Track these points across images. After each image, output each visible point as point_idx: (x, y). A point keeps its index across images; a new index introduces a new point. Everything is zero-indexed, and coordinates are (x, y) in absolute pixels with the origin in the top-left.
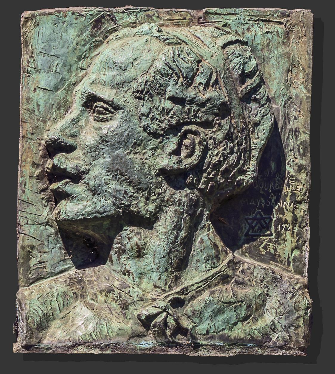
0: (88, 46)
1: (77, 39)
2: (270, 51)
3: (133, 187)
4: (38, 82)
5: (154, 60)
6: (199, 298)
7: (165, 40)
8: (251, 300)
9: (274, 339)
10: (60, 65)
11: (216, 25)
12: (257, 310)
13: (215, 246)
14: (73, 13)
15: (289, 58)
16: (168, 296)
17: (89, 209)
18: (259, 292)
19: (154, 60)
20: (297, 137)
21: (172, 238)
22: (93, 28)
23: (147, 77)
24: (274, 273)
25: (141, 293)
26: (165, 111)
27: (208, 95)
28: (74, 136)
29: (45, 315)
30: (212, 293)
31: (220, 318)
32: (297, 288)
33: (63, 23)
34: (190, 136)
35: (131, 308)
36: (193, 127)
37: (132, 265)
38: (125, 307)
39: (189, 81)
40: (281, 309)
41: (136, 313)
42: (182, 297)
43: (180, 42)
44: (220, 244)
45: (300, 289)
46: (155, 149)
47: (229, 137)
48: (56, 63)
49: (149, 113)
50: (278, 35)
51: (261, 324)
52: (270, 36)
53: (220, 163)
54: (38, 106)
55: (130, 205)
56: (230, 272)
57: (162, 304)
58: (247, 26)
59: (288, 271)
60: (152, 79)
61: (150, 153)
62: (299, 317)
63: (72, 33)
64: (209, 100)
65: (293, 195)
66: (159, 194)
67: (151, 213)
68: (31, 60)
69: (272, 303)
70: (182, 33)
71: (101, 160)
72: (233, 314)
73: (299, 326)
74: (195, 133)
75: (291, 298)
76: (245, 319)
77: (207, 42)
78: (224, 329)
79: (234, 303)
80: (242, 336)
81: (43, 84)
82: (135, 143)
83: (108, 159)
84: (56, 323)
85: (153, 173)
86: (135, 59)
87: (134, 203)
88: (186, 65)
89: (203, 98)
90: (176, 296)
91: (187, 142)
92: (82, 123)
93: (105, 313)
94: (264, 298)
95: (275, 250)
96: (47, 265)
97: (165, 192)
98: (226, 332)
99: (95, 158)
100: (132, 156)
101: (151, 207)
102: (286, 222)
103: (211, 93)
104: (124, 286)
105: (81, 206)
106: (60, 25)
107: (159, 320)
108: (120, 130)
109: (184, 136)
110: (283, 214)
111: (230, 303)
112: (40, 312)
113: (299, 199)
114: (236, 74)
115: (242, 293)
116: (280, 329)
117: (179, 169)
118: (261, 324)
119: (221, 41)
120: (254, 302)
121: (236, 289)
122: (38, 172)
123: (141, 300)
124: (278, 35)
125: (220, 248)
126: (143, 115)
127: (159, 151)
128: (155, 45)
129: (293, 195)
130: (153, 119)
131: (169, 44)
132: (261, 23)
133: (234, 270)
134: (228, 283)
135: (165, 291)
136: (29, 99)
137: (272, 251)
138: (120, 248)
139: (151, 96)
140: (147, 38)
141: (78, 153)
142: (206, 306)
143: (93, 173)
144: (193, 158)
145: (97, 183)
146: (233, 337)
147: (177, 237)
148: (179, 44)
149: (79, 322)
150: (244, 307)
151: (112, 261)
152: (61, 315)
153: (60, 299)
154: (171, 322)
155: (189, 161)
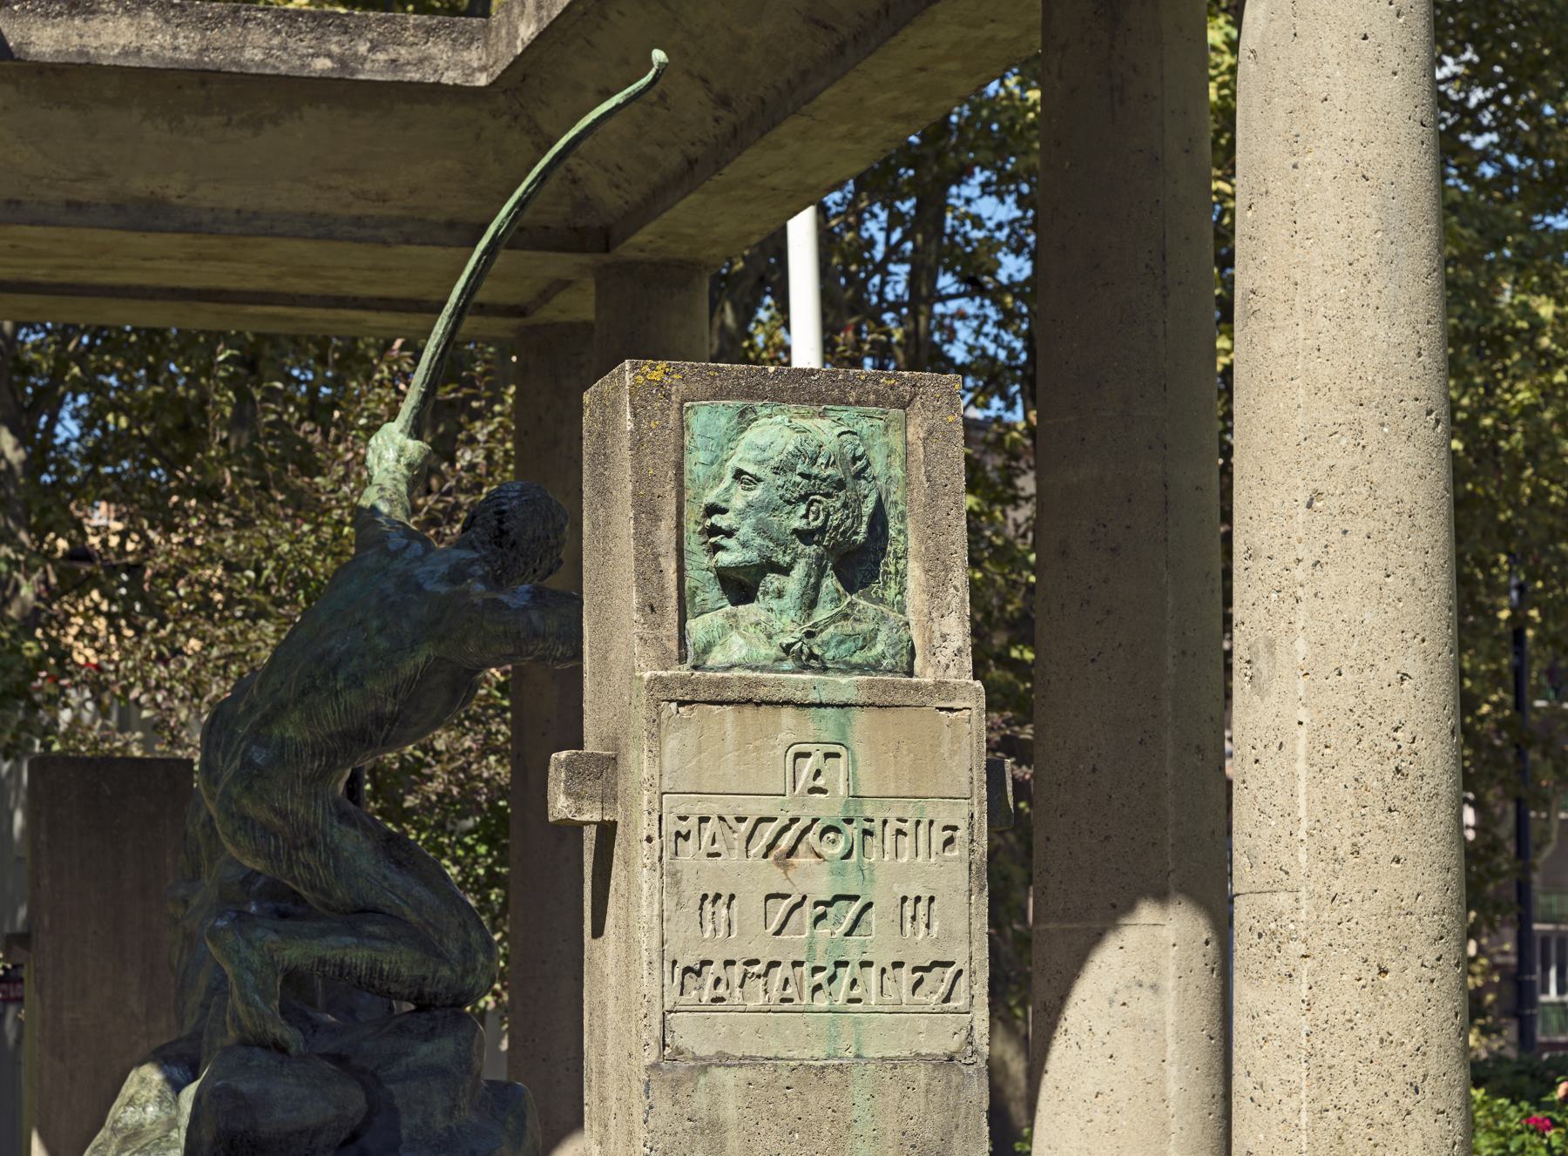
13: (838, 591)
21: (804, 583)
23: (781, 457)
26: (796, 484)
31: (843, 647)
36: (818, 497)
37: (774, 604)
38: (770, 637)
39: (814, 461)
47: (845, 506)
51: (874, 652)
53: (839, 526)
56: (849, 612)
63: (723, 420)
64: (829, 476)
65: (895, 552)
69: (881, 636)
70: (807, 423)
71: (748, 521)
74: (820, 502)
84: (716, 649)
89: (825, 474)
91: (813, 508)
92: (733, 491)
93: (755, 641)
99: (743, 519)
101: (788, 559)
103: (830, 471)
104: (769, 620)
107: (796, 647)
109: (811, 504)
118: (874, 652)
122: (699, 528)
128: (787, 432)
129: (895, 552)
136: (691, 471)
142: (832, 638)
143: (742, 531)
149: (735, 648)
154: (806, 650)
155: (815, 523)
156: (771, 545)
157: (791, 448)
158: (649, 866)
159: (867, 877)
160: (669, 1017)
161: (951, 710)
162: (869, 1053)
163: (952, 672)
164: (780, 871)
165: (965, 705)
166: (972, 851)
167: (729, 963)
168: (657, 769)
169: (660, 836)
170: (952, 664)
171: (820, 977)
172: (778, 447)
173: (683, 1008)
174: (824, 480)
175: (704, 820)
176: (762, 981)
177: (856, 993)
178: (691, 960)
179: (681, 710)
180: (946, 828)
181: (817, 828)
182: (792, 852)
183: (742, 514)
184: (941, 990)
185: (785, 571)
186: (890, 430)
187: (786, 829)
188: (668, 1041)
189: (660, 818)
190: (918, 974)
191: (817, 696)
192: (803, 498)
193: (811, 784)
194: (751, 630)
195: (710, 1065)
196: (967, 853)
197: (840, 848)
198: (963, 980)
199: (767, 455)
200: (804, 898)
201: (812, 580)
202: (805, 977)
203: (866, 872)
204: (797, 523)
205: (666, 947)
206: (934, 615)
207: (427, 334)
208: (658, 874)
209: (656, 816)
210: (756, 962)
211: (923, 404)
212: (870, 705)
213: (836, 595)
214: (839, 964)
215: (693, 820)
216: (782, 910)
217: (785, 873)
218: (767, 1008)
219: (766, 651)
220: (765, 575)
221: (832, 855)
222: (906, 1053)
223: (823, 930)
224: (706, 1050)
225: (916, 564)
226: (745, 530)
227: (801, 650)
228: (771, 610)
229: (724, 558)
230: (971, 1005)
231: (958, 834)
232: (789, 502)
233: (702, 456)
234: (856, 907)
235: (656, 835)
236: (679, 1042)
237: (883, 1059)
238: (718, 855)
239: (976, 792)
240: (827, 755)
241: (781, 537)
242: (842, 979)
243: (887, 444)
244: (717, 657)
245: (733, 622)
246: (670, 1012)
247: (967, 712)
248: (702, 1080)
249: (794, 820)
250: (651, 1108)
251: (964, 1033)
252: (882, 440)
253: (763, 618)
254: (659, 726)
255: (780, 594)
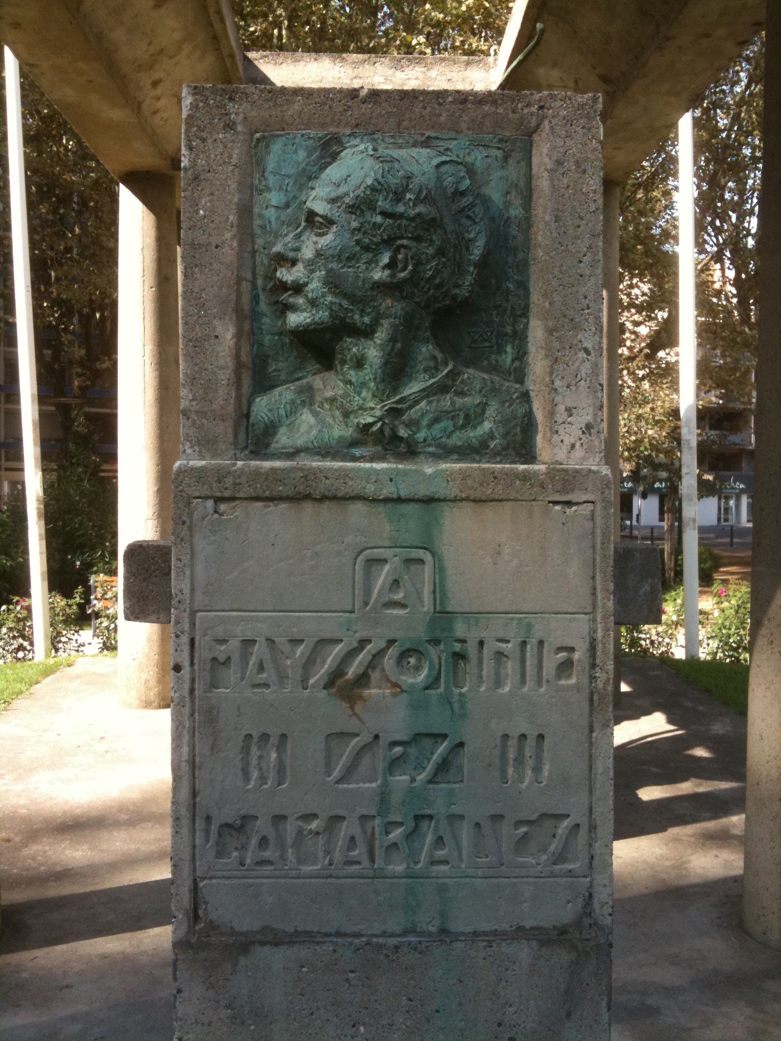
0: (317, 167)
1: (307, 160)
2: (489, 175)
3: (348, 300)
4: (270, 200)
5: (366, 176)
6: (418, 407)
7: (378, 158)
8: (469, 410)
9: (492, 446)
10: (291, 184)
11: (438, 149)
12: (476, 418)
13: (434, 358)
14: (302, 135)
15: (507, 180)
16: (385, 406)
17: (308, 320)
18: (479, 401)
19: (366, 176)
20: (516, 255)
21: (388, 349)
22: (322, 150)
23: (359, 192)
24: (493, 383)
25: (361, 402)
26: (376, 226)
27: (417, 210)
28: (297, 249)
29: (272, 422)
30: (430, 403)
31: (437, 426)
32: (514, 397)
33: (293, 144)
34: (402, 250)
35: (352, 416)
36: (405, 242)
37: (352, 375)
38: (346, 415)
39: (398, 197)
40: (499, 417)
41: (356, 421)
42: (400, 406)
43: (392, 160)
44: (440, 356)
45: (517, 398)
46: (369, 263)
47: (440, 252)
48: (287, 182)
49: (361, 227)
50: (497, 160)
51: (480, 431)
52: (489, 160)
53: (433, 277)
54: (270, 222)
55: (345, 318)
56: (450, 383)
57: (378, 413)
58: (467, 151)
59: (509, 381)
60: (362, 195)
61: (364, 267)
62: (516, 425)
63: (302, 155)
64: (419, 215)
65: (513, 309)
66: (374, 307)
67: (367, 325)
68: (262, 179)
69: (491, 412)
70: (396, 153)
71: (318, 274)
72: (450, 423)
73: (516, 434)
74: (406, 247)
75: (509, 407)
76: (463, 427)
77: (421, 162)
78: (441, 437)
79: (451, 412)
80: (459, 443)
81: (274, 202)
82: (348, 257)
83: (323, 273)
84: (282, 430)
85: (367, 286)
86: (349, 176)
87: (350, 315)
88: (395, 181)
89: (412, 213)
90: (395, 406)
91: (400, 257)
92: (304, 238)
93: (330, 420)
94: (483, 406)
95: (497, 361)
96: (283, 373)
97: (381, 305)
98: (443, 440)
99: (312, 271)
100: (345, 270)
101: (367, 319)
102: (506, 334)
103: (421, 209)
104: (346, 395)
105: (302, 318)
106: (290, 147)
107: (375, 429)
108: (333, 244)
109: (397, 251)
110: (504, 327)
111: (447, 412)
112: (266, 418)
113: (518, 313)
114: (450, 190)
115: (459, 401)
116: (498, 436)
117: (392, 283)
118: (480, 431)
119: (435, 162)
120: (472, 411)
121: (455, 398)
122: (270, 285)
123: (361, 408)
124: (497, 160)
125: (440, 360)
126: (354, 229)
127: (373, 265)
128: (370, 162)
129: (513, 309)
130: (365, 233)
131: (382, 162)
132: (481, 148)
133: (454, 380)
134: (447, 392)
135: (383, 401)
136: (261, 216)
137: (494, 362)
138: (342, 359)
139: (362, 211)
140: (361, 156)
141: (300, 266)
142: (423, 415)
143: (311, 286)
144: (407, 272)
145: (315, 295)
146: (450, 445)
147: (392, 349)
148: (391, 162)
149: (303, 428)
150: (462, 415)
151: (336, 370)
152: (288, 422)
153: (288, 407)
154: (387, 432)
155: (403, 275)
156: (345, 303)
157: (369, 181)
158: (176, 700)
159: (457, 710)
160: (201, 885)
161: (569, 504)
162: (458, 925)
163: (578, 453)
164: (345, 705)
165: (584, 498)
166: (593, 678)
167: (279, 819)
168: (188, 581)
169: (192, 664)
170: (578, 445)
171: (396, 834)
172: (354, 181)
173: (220, 874)
174: (412, 219)
175: (248, 643)
176: (321, 840)
177: (441, 853)
178: (228, 815)
179: (223, 507)
180: (561, 649)
181: (393, 652)
182: (363, 679)
183: (311, 265)
184: (552, 848)
185: (367, 333)
186: (511, 161)
187: (352, 654)
188: (201, 912)
189: (192, 642)
190: (523, 829)
191: (394, 489)
192: (388, 242)
193: (386, 599)
194: (327, 406)
195: (253, 943)
196: (586, 680)
197: (421, 677)
198: (582, 836)
199: (342, 190)
200: (377, 737)
201: (399, 345)
202: (377, 836)
203: (456, 706)
204: (378, 275)
205: (198, 800)
206: (558, 383)
207: (601, 310)
208: (187, 710)
209: (185, 639)
210: (315, 816)
211: (552, 128)
212: (462, 500)
213: (432, 364)
214: (418, 818)
215: (234, 644)
216: (347, 753)
217: (352, 707)
218: (327, 872)
219: (340, 431)
220: (341, 339)
221: (412, 686)
222: (505, 926)
223: (401, 779)
224: (246, 923)
225: (540, 323)
226: (315, 286)
227: (381, 430)
228: (350, 382)
229: (294, 319)
230: (591, 866)
231: (576, 656)
232: (366, 248)
233: (275, 198)
234: (442, 748)
235: (186, 664)
236: (213, 916)
237: (475, 933)
238: (266, 685)
239: (600, 603)
240: (409, 561)
241: (359, 293)
242: (426, 835)
243: (506, 178)
244: (283, 439)
245: (308, 397)
246: (203, 879)
247: (590, 507)
248: (243, 961)
249: (363, 642)
250: (179, 991)
251: (580, 903)
252: (499, 173)
253: (341, 392)
254: (190, 528)
255: (359, 363)
